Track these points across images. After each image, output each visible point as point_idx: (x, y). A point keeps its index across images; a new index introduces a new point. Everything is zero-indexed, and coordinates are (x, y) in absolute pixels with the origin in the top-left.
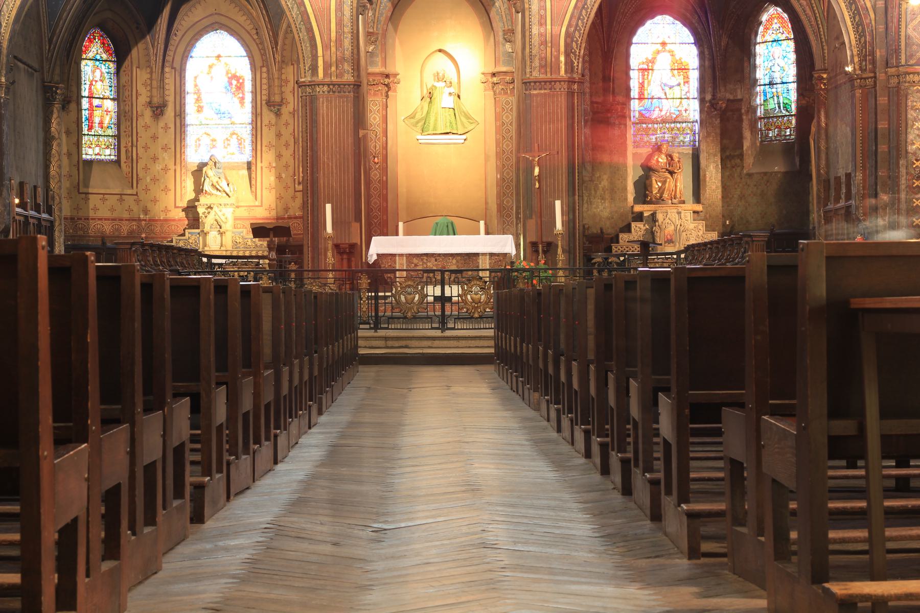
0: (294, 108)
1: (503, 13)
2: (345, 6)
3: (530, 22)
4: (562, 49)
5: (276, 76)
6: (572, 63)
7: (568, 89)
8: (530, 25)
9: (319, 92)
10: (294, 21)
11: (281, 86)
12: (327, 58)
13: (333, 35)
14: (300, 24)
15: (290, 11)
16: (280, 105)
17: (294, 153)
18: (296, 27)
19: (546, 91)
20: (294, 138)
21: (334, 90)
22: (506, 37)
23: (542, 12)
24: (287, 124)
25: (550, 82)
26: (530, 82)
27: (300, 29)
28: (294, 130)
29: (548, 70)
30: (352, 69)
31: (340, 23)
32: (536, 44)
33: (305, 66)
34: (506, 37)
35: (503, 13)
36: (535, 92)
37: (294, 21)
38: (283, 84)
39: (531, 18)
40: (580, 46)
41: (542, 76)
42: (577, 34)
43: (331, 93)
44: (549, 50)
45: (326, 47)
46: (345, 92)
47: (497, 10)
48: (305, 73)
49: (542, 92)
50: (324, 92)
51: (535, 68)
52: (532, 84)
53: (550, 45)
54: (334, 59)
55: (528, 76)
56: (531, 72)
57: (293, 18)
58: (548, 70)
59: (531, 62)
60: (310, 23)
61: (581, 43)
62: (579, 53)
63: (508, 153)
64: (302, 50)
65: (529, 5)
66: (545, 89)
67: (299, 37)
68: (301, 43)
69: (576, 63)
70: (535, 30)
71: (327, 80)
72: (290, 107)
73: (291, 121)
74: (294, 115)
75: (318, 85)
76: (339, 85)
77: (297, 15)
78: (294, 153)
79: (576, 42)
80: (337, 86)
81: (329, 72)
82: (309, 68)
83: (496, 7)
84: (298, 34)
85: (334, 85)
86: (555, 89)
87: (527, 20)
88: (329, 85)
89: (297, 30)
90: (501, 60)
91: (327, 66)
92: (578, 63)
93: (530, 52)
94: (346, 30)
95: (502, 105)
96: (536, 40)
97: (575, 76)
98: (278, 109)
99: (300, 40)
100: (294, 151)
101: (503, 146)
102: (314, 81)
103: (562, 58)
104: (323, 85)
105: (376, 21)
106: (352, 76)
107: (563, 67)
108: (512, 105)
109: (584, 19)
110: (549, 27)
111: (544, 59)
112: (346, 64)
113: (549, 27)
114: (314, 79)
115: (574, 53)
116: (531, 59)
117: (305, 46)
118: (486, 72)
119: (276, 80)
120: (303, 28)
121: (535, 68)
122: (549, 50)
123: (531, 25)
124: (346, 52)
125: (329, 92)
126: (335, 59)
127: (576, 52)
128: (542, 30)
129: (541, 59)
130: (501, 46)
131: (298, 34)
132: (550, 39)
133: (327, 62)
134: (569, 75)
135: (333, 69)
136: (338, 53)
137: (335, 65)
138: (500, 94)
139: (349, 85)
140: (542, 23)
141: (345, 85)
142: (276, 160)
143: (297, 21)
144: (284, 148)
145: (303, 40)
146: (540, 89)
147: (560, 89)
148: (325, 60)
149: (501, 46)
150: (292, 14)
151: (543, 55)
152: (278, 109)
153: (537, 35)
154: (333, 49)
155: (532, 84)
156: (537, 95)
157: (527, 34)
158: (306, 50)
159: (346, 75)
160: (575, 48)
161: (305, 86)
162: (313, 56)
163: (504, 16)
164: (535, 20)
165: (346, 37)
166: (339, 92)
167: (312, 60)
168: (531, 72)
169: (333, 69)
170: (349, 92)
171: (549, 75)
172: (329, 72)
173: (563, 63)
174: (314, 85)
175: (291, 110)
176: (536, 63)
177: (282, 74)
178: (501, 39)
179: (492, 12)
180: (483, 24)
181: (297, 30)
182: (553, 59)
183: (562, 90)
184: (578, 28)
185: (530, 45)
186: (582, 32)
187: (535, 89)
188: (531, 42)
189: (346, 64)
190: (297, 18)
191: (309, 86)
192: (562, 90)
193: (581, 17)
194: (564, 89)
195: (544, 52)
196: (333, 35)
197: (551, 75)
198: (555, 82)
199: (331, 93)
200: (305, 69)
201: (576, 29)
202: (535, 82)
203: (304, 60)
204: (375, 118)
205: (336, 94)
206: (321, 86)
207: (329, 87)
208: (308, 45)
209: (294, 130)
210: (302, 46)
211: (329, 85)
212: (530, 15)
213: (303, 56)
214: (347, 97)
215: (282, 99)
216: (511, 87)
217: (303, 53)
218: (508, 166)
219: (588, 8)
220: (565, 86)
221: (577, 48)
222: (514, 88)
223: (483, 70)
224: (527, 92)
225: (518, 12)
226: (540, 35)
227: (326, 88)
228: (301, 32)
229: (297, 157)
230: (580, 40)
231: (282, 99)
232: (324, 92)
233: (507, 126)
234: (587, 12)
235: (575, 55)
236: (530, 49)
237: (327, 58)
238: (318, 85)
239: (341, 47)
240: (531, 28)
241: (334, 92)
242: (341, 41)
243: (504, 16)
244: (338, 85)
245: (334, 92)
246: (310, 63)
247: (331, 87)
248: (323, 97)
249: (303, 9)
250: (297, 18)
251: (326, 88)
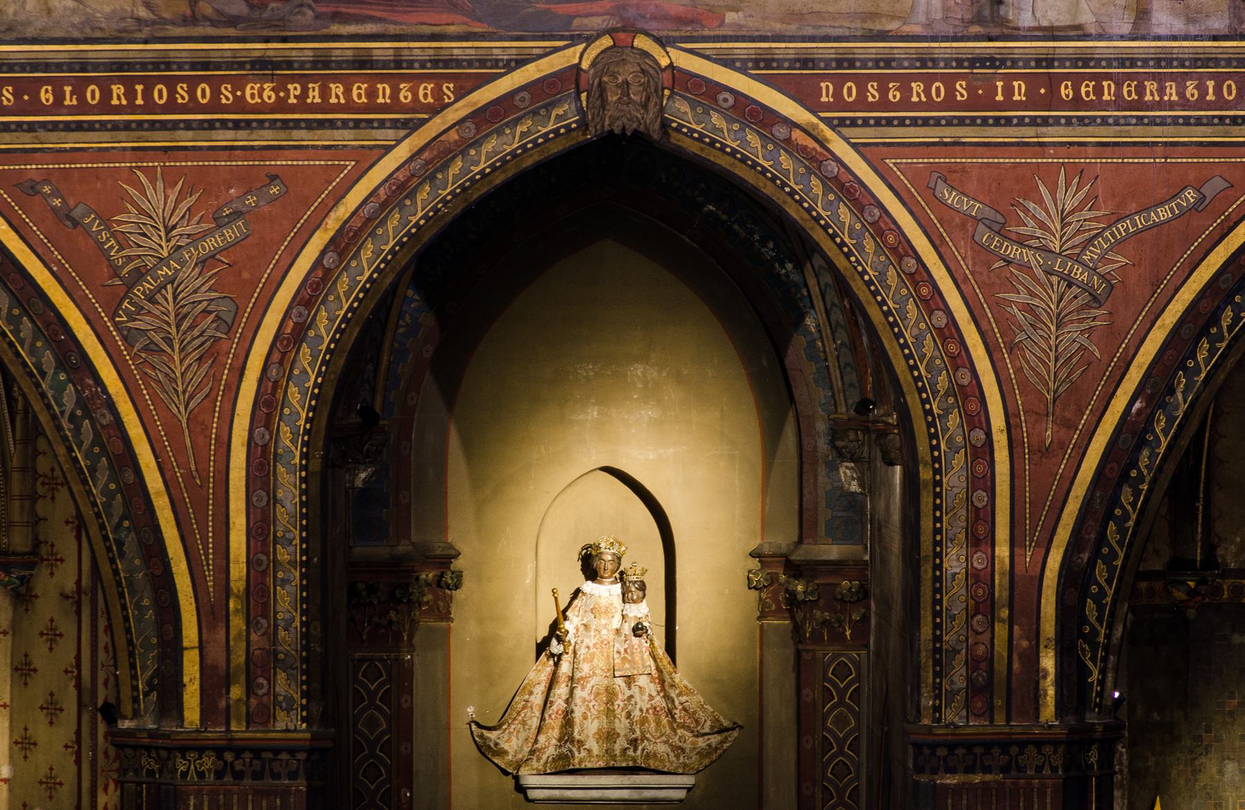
0: (79, 582)
1: (832, 363)
2: (281, 469)
3: (937, 531)
4: (1049, 627)
5: (16, 462)
6: (1085, 672)
7: (1066, 768)
8: (937, 543)
9: (184, 774)
10: (98, 515)
11: (34, 497)
12: (216, 654)
13: (238, 570)
14: (118, 527)
15: (85, 482)
16: (32, 566)
17: (78, 741)
18: (106, 538)
19: (988, 777)
20: (78, 686)
21: (238, 766)
22: (840, 444)
23: (981, 497)
24: (52, 635)
25: (1005, 745)
26: (934, 746)
27: (120, 544)
28: (78, 658)
29: (999, 702)
30: (304, 694)
31: (260, 530)
32: (958, 609)
33: (134, 677)
34: (840, 444)
35: (832, 363)
36: (951, 780)
37: (98, 515)
38: (41, 490)
39: (940, 520)
40: (1112, 614)
41: (976, 725)
42: (1101, 572)
43: (228, 779)
44: (1001, 631)
45: (212, 615)
46: (276, 776)
47: (812, 344)
48: (135, 700)
49: (977, 778)
50: (201, 775)
51: (952, 694)
52: (942, 752)
53: (1005, 613)
54: (239, 657)
55: (926, 721)
56: (937, 709)
57: (94, 504)
58: (999, 702)
59: (937, 674)
60: (157, 529)
61: (1114, 602)
62: (1108, 637)
63: (841, 748)
64: (126, 619)
65: (937, 472)
66: (987, 770)
67: (116, 572)
68: (122, 596)
69: (1096, 675)
70: (955, 562)
71: (216, 732)
72: (66, 576)
73: (67, 627)
74: (79, 604)
75: (183, 750)
76: (257, 752)
77: (109, 495)
78: (78, 741)
79: (1099, 598)
80: (247, 756)
81: (223, 704)
82: (149, 683)
83: (807, 332)
84: (112, 561)
85: (239, 752)
86: (1021, 769)
87: (927, 524)
88: (219, 751)
89: (109, 549)
90: (822, 519)
91: (214, 682)
92: (1103, 672)
93: (937, 639)
94: (283, 554)
95: (825, 678)
96: (956, 598)
97: (1091, 718)
98: (21, 579)
99: (119, 584)
100: (78, 733)
101: (824, 773)
102: (166, 736)
103: (1048, 662)
104: (201, 750)
105: (381, 384)
106: (303, 720)
107: (1051, 692)
108: (858, 678)
109: (1126, 517)
110: (1003, 551)
111: (983, 665)
112: (281, 676)
113: (1003, 551)
114: (169, 727)
115: (1091, 639)
116: (937, 662)
117: (138, 606)
118: (767, 550)
119: (16, 477)
120: (130, 541)
121: (952, 694)
122: (1001, 631)
123: (940, 543)
124: (282, 633)
125: (219, 774)
126: (242, 659)
127: (1095, 632)
128: (979, 562)
129: (973, 663)
130: (822, 470)
131: (112, 561)
132: (1006, 594)
133: (215, 668)
134: (1071, 720)
135: (237, 692)
136: (254, 637)
137: (243, 678)
138: (816, 638)
139: (292, 752)
140: (981, 537)
141: (277, 751)
142: (11, 757)
143: (109, 516)
144: (42, 717)
145: (130, 584)
146: (970, 770)
147: (1039, 769)
148: (209, 661)
149: (822, 470)
150: (89, 493)
151: (981, 650)
152: (21, 579)
153: (961, 576)
154: (237, 623)
155: (942, 752)
156: (957, 790)
157: (927, 573)
158: (139, 620)
159: (281, 715)
160: (1093, 620)
161: (135, 747)
162: (162, 643)
163: (835, 374)
164: (956, 524)
165: (284, 582)
166: (257, 776)
167: (161, 659)
168: (937, 709)
169: (237, 692)
170: (293, 776)
171: (1000, 720)
172: (223, 704)
173: (1051, 677)
174: (169, 750)
175: (70, 586)
176: (958, 677)
177: (36, 453)
178: (823, 445)
179: (791, 350)
180: (764, 449)
181: (109, 549)
182: (1016, 666)
183: (1047, 771)
184: (1105, 550)
185: (936, 614)
186: (1119, 563)
187: (952, 771)
188: (940, 602)
189: (281, 676)
190: (108, 506)
191: (148, 748)
192: (1047, 771)
193: (1118, 512)
194: (1054, 769)
195: (986, 637)
196: (238, 570)
197: (1008, 719)
198: (1023, 745)
199: (228, 779)
200: (135, 688)
201: (1096, 554)
202: (952, 747)
203: (131, 654)
204: (372, 723)
205: (248, 782)
206: (192, 755)
207: (220, 756)
208: (146, 602)
209: (78, 658)
210: (124, 607)
211: (219, 751)
212: (937, 507)
213: (130, 643)
214: (285, 794)
215: (37, 543)
216: (856, 617)
217: (128, 631)
218: (842, 698)
219: (1141, 478)
220: (1058, 761)
221: (1100, 619)
222: (865, 618)
223: (754, 544)
224: (923, 779)
225: (891, 464)
226: (973, 577)
227: (208, 762)
228: (122, 554)
229: (87, 755)
230: (1110, 592)
231: (37, 543)
232: (201, 775)
233: (841, 751)
234: (1137, 493)
235: (1094, 646)
236: (937, 626)
237: (216, 654)
238: (183, 750)
239: (265, 615)
240: (939, 555)
241: (238, 776)
242: (264, 592)
243: (835, 374)
244: (252, 750)
245: (238, 776)
246: (152, 665)
247: (229, 757)
248: (199, 794)
249: (129, 476)
250: (108, 506)
251: (208, 762)
